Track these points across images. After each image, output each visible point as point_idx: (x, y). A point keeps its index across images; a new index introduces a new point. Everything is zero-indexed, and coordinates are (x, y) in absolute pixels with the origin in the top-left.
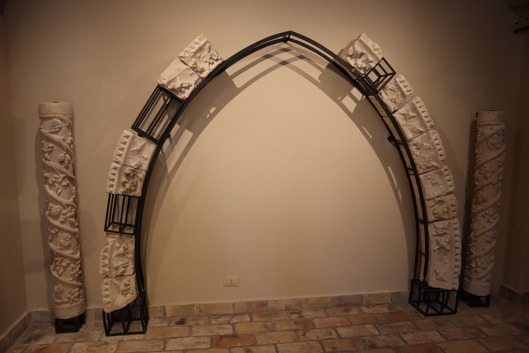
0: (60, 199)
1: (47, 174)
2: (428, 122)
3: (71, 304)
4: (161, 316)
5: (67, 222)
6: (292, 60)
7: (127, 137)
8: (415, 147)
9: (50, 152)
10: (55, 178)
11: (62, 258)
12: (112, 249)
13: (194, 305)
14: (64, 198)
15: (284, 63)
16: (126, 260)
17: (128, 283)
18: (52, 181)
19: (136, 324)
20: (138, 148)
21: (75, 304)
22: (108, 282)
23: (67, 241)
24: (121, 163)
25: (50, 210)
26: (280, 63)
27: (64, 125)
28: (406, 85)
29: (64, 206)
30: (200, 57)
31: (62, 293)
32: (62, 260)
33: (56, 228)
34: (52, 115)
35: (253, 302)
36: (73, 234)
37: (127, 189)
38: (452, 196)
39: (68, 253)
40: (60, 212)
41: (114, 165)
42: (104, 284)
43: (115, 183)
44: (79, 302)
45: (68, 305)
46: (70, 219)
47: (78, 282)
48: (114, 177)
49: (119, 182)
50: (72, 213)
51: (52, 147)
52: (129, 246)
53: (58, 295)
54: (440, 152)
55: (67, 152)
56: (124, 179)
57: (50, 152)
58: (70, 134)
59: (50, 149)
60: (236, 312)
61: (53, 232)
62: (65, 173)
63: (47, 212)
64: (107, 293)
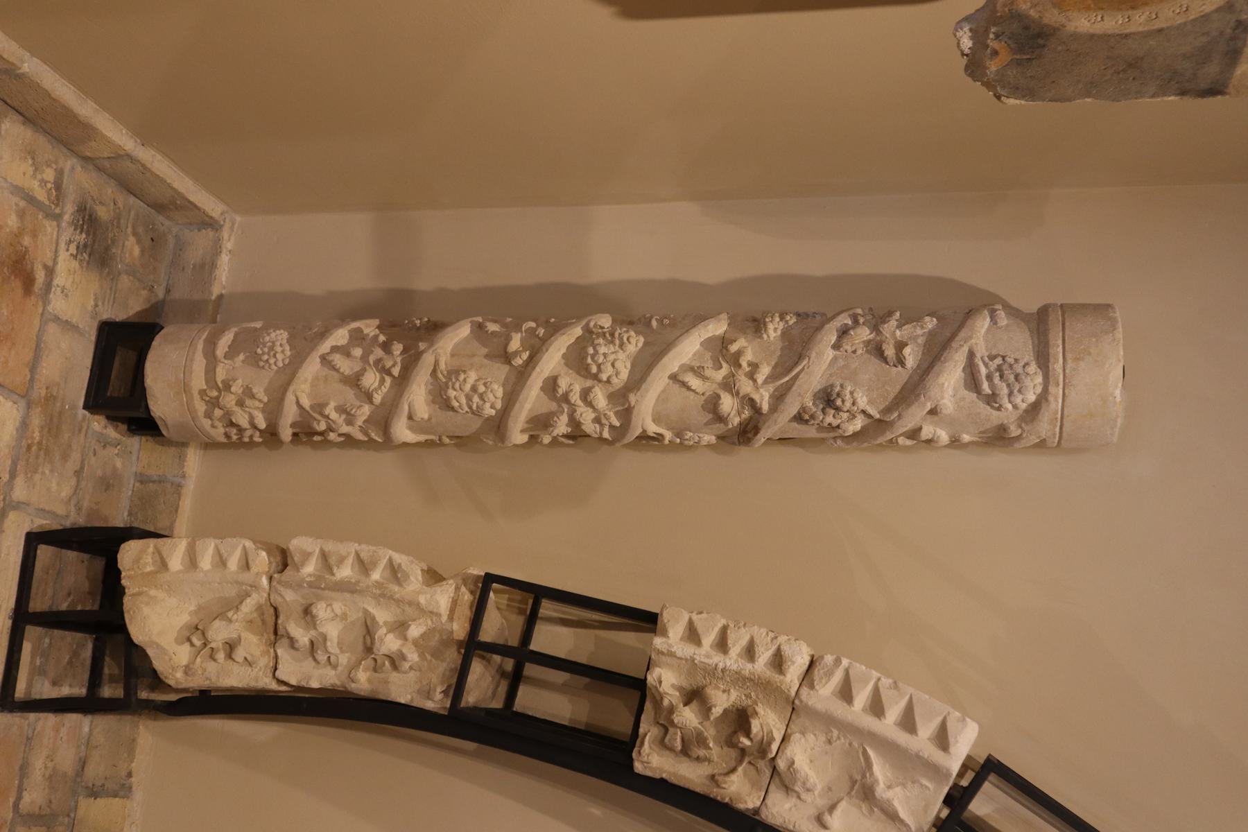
0: (658, 382)
1: (774, 330)
3: (202, 393)
5: (553, 406)
7: (942, 739)
9: (879, 352)
10: (754, 366)
12: (399, 602)
14: (663, 398)
16: (344, 659)
17: (240, 654)
18: (739, 353)
19: (75, 654)
20: (881, 791)
21: (201, 408)
22: (254, 569)
23: (469, 398)
24: (805, 691)
25: (610, 337)
27: (1008, 414)
29: (622, 398)
31: (255, 360)
32: (389, 373)
33: (531, 358)
34: (1058, 367)
36: (498, 426)
37: (671, 709)
39: (418, 396)
40: (596, 377)
41: (799, 658)
43: (705, 653)
44: (206, 423)
45: (198, 382)
46: (564, 418)
49: (711, 672)
50: (589, 427)
51: (901, 362)
52: (412, 675)
53: (248, 345)
55: (877, 426)
56: (722, 701)
57: (879, 352)
58: (966, 438)
59: (890, 351)
61: (515, 344)
62: (774, 408)
63: (605, 321)
64: (206, 563)
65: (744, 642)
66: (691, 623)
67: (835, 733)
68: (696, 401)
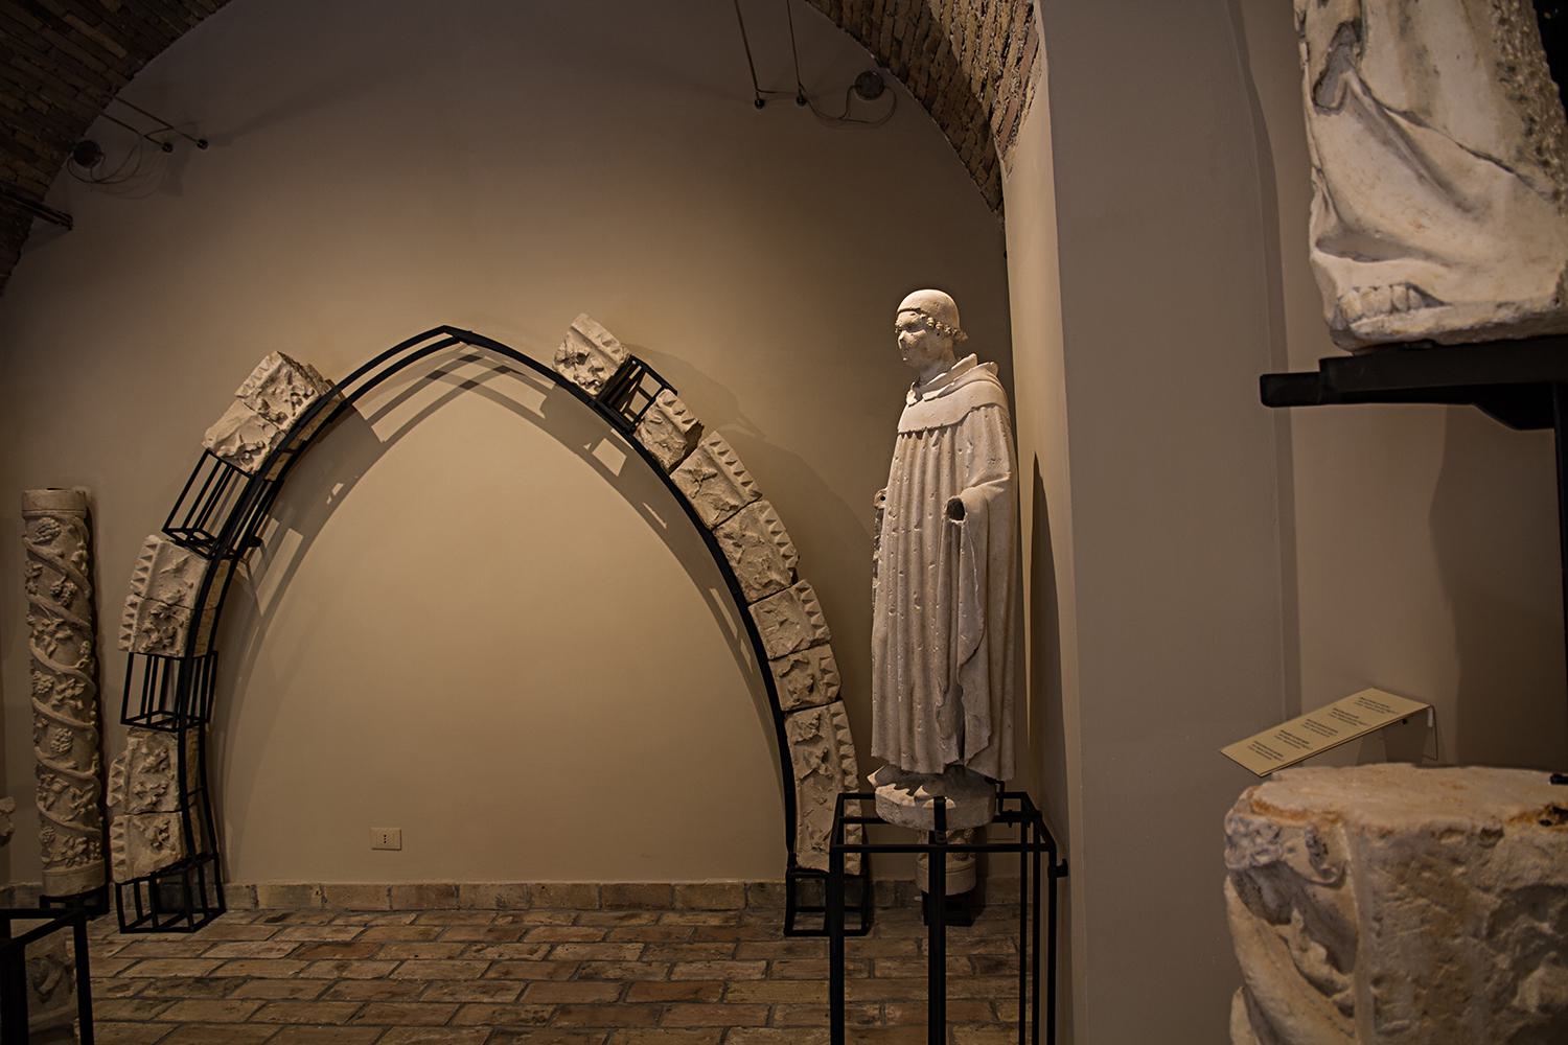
2: (745, 484)
4: (248, 906)
6: (486, 377)
7: (153, 546)
8: (731, 542)
11: (52, 776)
13: (311, 887)
14: (60, 662)
15: (469, 385)
18: (38, 631)
23: (63, 742)
26: (477, 384)
28: (678, 410)
30: (274, 393)
35: (428, 887)
38: (827, 650)
39: (64, 765)
41: (132, 598)
42: (116, 826)
45: (62, 869)
47: (86, 825)
48: (131, 621)
51: (39, 569)
54: (783, 550)
59: (35, 573)
60: (396, 907)
64: (121, 843)
65: (128, 618)
66: (123, 638)
67: (156, 584)
68: (61, 647)
